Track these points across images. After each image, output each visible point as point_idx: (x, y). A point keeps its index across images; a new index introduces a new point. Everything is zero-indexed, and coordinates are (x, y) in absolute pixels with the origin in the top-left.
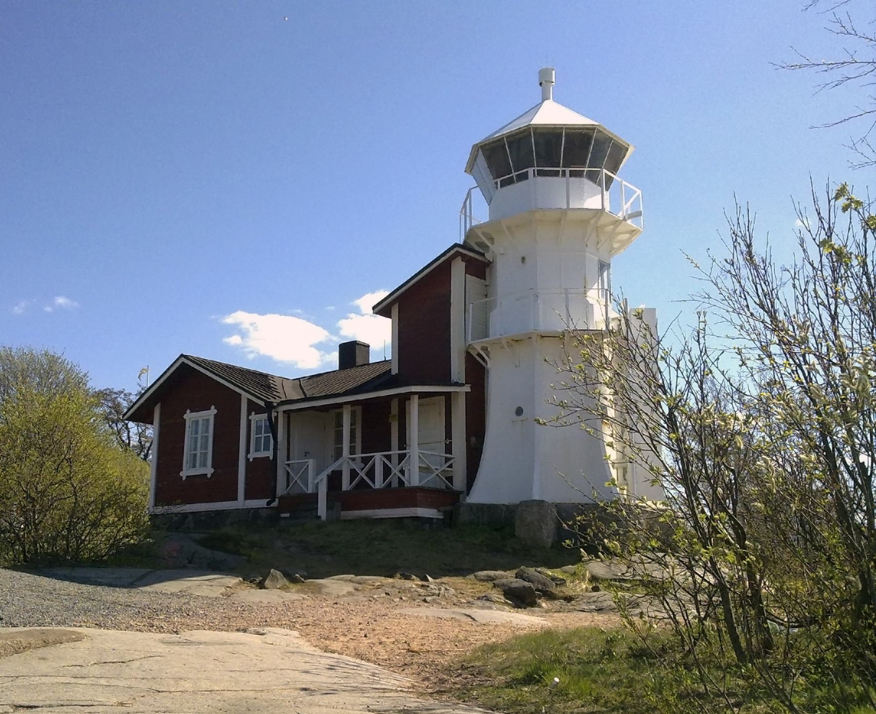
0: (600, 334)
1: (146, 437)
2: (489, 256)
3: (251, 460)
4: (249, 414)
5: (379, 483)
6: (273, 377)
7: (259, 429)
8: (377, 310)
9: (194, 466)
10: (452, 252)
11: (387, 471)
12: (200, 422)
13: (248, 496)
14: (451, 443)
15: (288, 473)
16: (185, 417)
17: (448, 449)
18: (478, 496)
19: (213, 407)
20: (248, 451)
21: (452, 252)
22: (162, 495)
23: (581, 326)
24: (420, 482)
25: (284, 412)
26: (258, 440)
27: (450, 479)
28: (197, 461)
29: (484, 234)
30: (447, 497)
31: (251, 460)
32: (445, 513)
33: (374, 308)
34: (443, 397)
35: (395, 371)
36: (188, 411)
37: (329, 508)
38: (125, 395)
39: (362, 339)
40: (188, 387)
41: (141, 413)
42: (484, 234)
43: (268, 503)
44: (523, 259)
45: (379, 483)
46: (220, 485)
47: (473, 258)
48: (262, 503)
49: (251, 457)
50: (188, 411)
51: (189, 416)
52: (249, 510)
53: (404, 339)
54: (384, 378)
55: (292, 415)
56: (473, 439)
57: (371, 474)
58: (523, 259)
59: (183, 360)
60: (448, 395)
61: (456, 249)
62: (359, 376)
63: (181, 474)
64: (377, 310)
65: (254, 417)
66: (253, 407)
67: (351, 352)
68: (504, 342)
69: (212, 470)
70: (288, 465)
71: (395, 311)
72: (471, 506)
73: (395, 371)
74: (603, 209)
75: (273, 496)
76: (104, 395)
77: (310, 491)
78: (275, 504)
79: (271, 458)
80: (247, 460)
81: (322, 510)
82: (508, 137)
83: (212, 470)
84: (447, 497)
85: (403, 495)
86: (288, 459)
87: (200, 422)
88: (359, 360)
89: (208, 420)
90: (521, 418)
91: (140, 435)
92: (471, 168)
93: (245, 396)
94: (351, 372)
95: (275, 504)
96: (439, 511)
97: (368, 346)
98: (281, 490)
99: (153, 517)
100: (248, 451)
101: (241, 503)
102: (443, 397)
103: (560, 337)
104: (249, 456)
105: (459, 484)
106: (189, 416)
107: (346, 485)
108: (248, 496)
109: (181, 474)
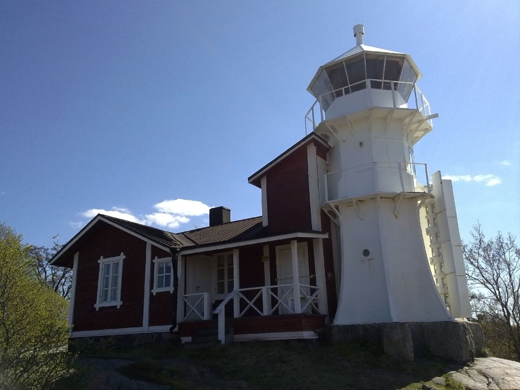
0: (414, 197)
1: (57, 276)
2: (331, 143)
3: (154, 294)
4: (153, 258)
5: (267, 310)
6: (164, 232)
7: (161, 270)
8: (251, 180)
9: (106, 299)
10: (310, 138)
11: (274, 301)
12: (111, 267)
13: (152, 323)
14: (314, 278)
15: (185, 303)
16: (99, 261)
17: (313, 282)
18: (342, 319)
19: (122, 254)
20: (152, 287)
21: (310, 138)
22: (79, 323)
23: (407, 190)
24: (302, 309)
25: (183, 256)
26: (160, 279)
27: (316, 305)
28: (109, 295)
29: (331, 126)
30: (320, 320)
31: (154, 294)
32: (319, 334)
33: (249, 179)
34: (306, 243)
35: (265, 224)
36: (102, 257)
37: (227, 332)
38: (45, 250)
39: (226, 206)
40: (103, 236)
41: (63, 259)
42: (331, 126)
43: (171, 329)
44: (361, 144)
45: (267, 310)
46: (129, 314)
47: (319, 143)
48: (166, 328)
49: (155, 291)
50: (102, 257)
51: (102, 261)
52: (152, 335)
53: (271, 202)
54: (254, 229)
55: (188, 258)
56: (330, 274)
57: (259, 303)
58: (361, 144)
59: (100, 218)
60: (310, 241)
61: (313, 136)
62: (222, 233)
63: (95, 306)
64: (251, 180)
65: (156, 260)
66: (157, 253)
67: (218, 215)
68: (354, 201)
69: (121, 303)
70: (186, 297)
71: (264, 182)
72: (338, 326)
73: (265, 224)
74: (418, 109)
75: (172, 320)
76: (30, 250)
77: (206, 317)
78: (176, 329)
79: (171, 292)
80: (151, 294)
81: (221, 336)
82: (346, 61)
83: (121, 303)
84: (320, 320)
85: (293, 322)
86: (185, 294)
87: (111, 267)
88: (225, 220)
89: (117, 264)
90: (369, 257)
91: (53, 275)
92: (312, 88)
93: (150, 243)
94: (219, 228)
95: (176, 329)
96: (315, 332)
97: (230, 211)
98: (180, 318)
99: (74, 345)
100: (152, 287)
101: (146, 328)
102: (306, 243)
103: (394, 198)
104: (152, 291)
105: (323, 309)
106: (102, 261)
107: (237, 314)
108: (152, 323)
109: (95, 306)
